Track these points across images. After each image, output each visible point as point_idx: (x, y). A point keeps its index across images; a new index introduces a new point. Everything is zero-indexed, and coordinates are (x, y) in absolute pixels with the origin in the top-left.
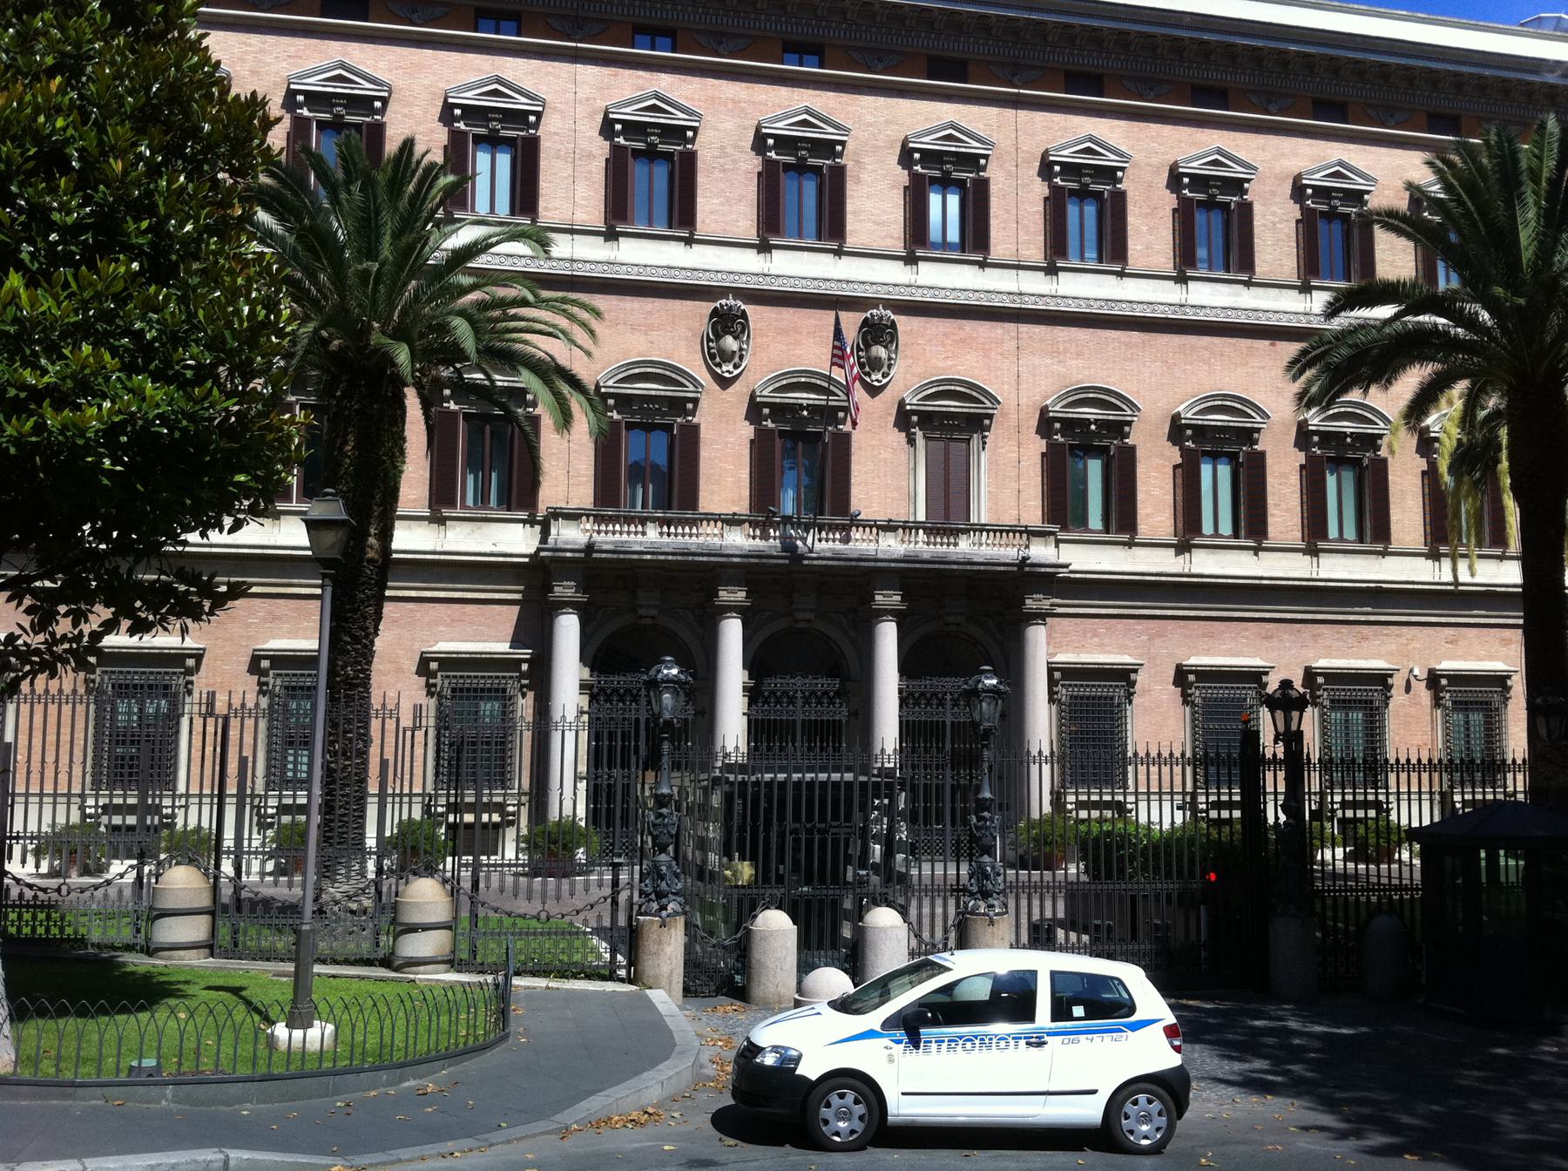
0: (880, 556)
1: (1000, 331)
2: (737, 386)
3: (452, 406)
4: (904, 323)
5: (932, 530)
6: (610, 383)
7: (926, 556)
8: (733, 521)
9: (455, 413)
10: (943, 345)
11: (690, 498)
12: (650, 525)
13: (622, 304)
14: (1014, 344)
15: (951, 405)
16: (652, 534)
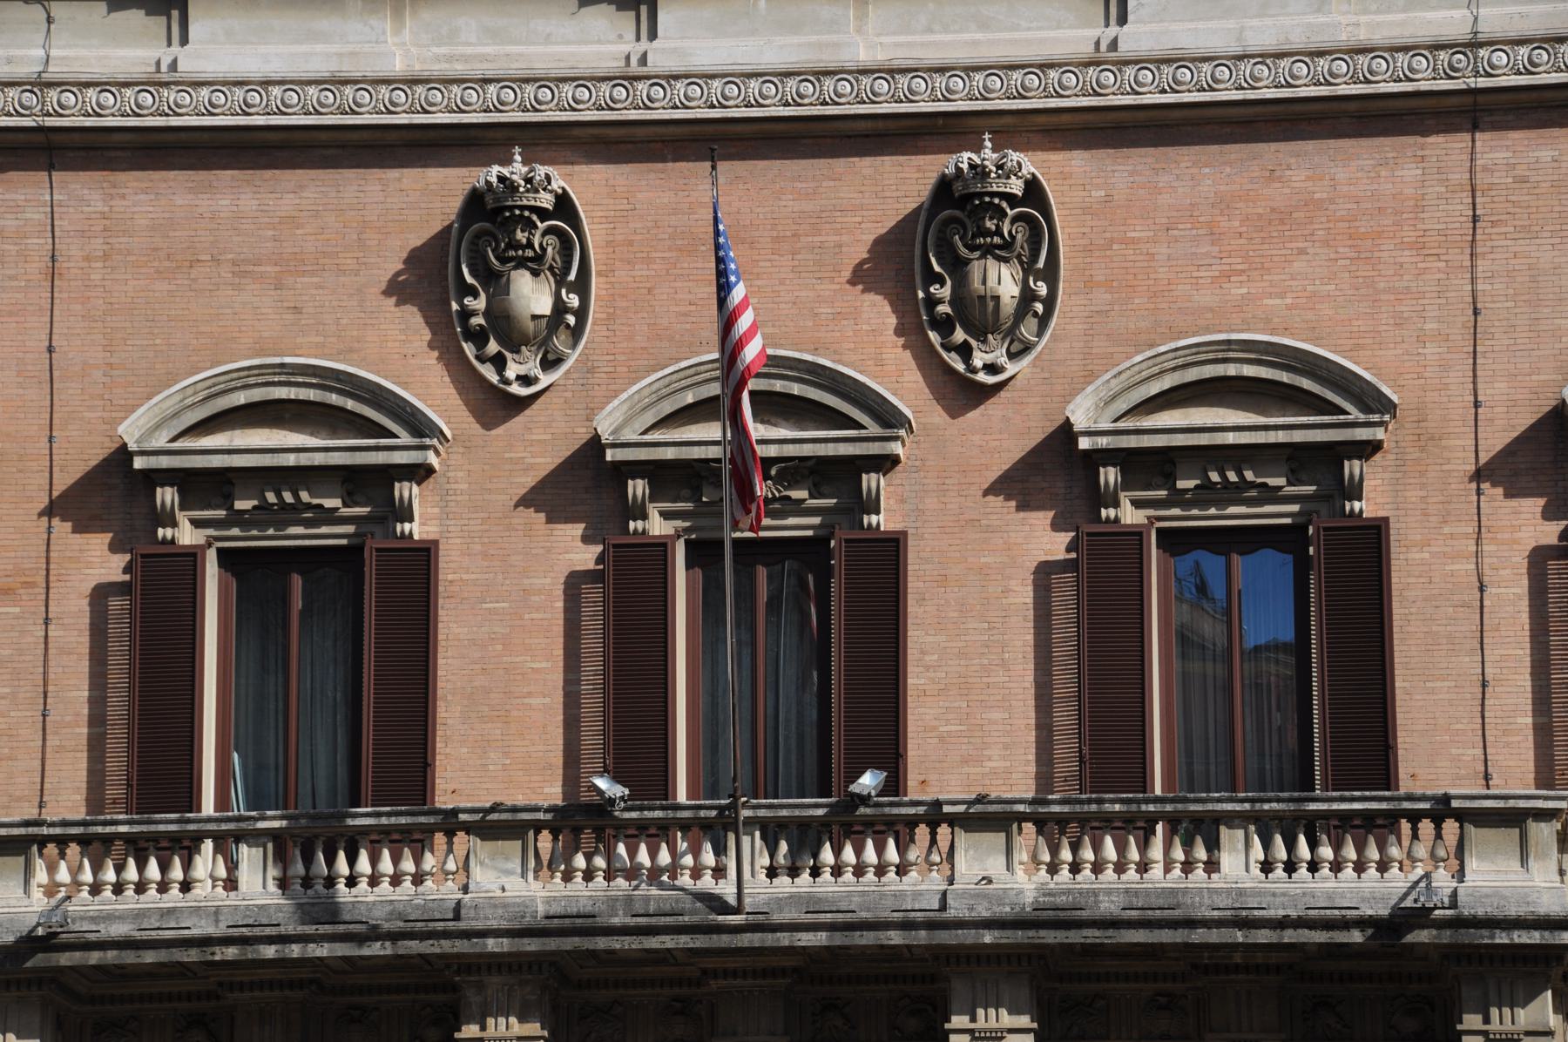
0: (956, 910)
1: (1410, 172)
2: (992, 409)
3: (1130, 515)
4: (1072, 180)
5: (579, 823)
6: (160, 441)
7: (1109, 906)
8: (988, 817)
9: (1136, 535)
10: (1215, 236)
11: (1368, 748)
12: (1231, 838)
13: (204, 203)
14: (1460, 207)
15: (1227, 423)
16: (1238, 869)
